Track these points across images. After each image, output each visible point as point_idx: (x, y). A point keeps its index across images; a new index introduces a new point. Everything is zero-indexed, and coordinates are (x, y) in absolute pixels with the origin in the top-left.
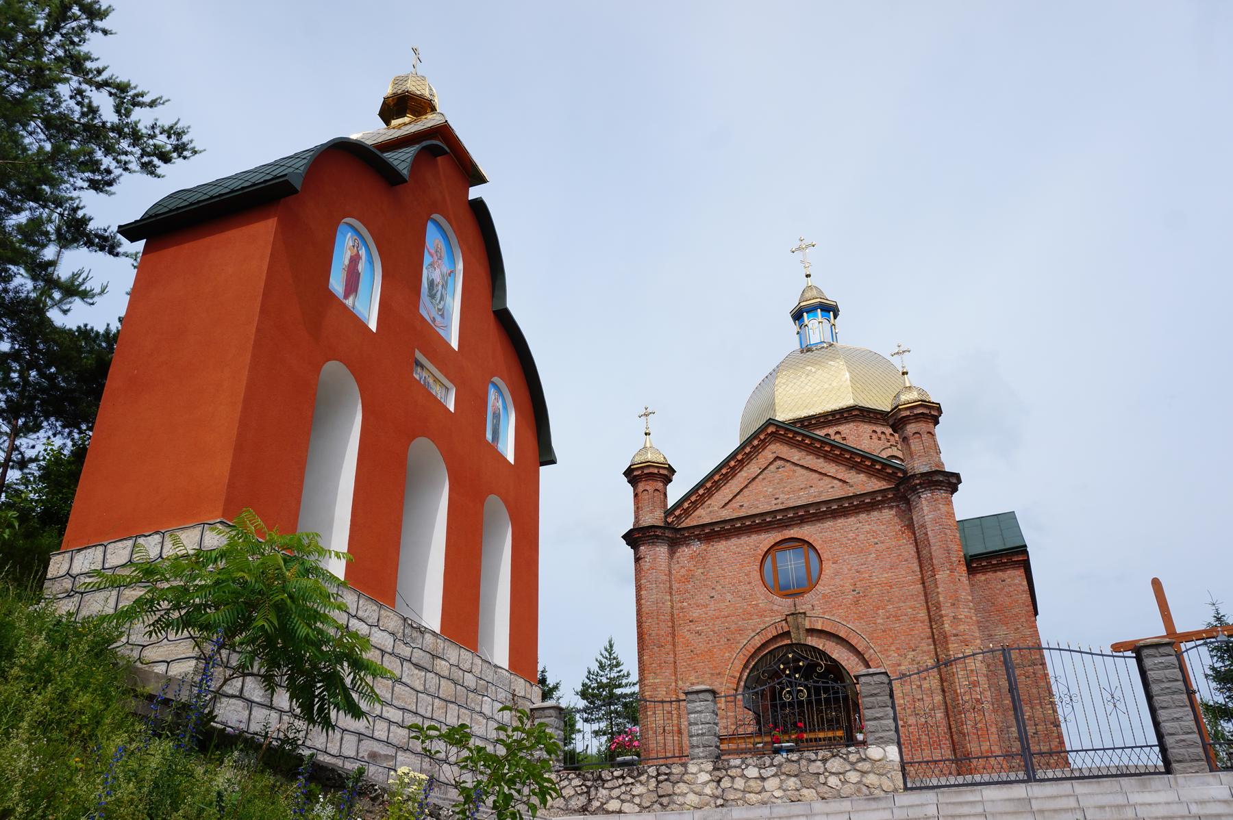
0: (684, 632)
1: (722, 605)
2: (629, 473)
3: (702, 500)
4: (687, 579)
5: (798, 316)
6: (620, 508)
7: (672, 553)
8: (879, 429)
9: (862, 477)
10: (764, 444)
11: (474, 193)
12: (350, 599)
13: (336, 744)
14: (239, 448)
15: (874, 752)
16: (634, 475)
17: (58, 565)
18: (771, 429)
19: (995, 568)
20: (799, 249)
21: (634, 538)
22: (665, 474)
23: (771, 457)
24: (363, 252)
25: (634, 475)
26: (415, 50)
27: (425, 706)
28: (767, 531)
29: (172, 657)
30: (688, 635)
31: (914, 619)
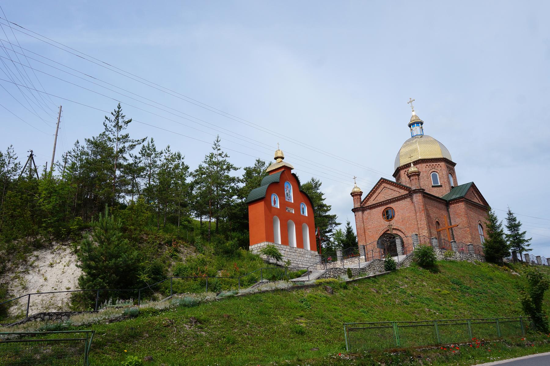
0: (367, 231)
2: (351, 194)
3: (368, 199)
5: (410, 126)
6: (351, 203)
7: (363, 213)
8: (428, 164)
9: (403, 191)
10: (381, 184)
11: (292, 171)
12: (282, 246)
13: (280, 263)
15: (361, 257)
16: (353, 194)
17: (250, 247)
19: (456, 203)
21: (354, 210)
22: (361, 194)
25: (353, 194)
26: (278, 144)
29: (265, 257)
31: (415, 224)
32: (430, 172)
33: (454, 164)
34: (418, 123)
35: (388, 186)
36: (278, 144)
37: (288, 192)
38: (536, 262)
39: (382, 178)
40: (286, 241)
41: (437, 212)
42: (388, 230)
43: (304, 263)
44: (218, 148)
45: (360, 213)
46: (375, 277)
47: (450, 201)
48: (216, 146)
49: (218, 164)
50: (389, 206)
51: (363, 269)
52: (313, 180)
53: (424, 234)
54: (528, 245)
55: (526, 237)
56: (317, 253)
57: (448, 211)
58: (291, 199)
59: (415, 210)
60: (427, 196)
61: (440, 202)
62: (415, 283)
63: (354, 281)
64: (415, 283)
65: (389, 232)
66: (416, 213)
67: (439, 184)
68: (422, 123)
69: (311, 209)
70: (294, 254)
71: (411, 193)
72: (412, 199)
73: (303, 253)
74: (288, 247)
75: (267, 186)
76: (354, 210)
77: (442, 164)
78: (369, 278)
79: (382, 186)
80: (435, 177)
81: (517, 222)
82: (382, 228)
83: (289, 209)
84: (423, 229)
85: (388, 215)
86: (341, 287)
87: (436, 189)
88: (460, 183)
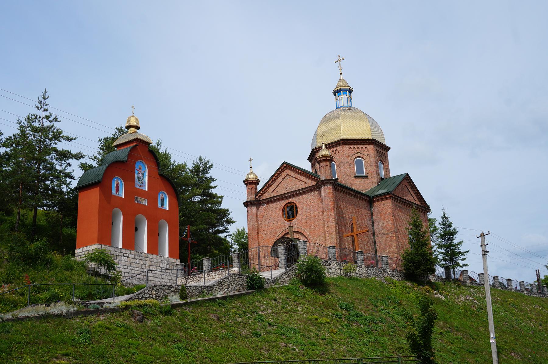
0: (261, 234)
1: (272, 225)
4: (263, 216)
6: (243, 194)
7: (258, 209)
8: (352, 147)
10: (283, 170)
12: (123, 251)
14: (99, 231)
17: (76, 251)
18: (285, 165)
20: (338, 61)
21: (247, 204)
23: (285, 174)
24: (119, 182)
25: (247, 182)
26: (133, 107)
27: (143, 267)
28: (284, 200)
29: (92, 265)
30: (263, 235)
32: (354, 157)
33: (387, 149)
34: (345, 90)
35: (292, 173)
36: (133, 107)
37: (140, 175)
38: (478, 280)
39: (284, 163)
40: (130, 243)
41: (353, 211)
42: (288, 233)
43: (156, 275)
44: (45, 107)
45: (254, 208)
46: (224, 298)
47: (374, 197)
48: (42, 104)
49: (43, 130)
50: (291, 200)
51: (209, 287)
52: (201, 160)
53: (332, 240)
54: (464, 259)
55: (462, 249)
56: (178, 261)
57: (371, 211)
58: (144, 186)
59: (323, 208)
60: (339, 187)
61: (360, 198)
62: (284, 308)
63: (187, 303)
64: (284, 308)
65: (289, 236)
66: (323, 212)
67: (365, 174)
68: (350, 91)
69: (175, 201)
70: (141, 262)
71: (319, 185)
72: (320, 193)
73: (156, 261)
74: (134, 252)
75: (106, 166)
76: (247, 204)
77: (371, 147)
78: (214, 300)
79: (284, 174)
80: (359, 164)
81: (451, 229)
82: (280, 230)
83: (140, 199)
84: (330, 234)
85: (291, 212)
86: (161, 312)
87: (359, 180)
88: (392, 175)
